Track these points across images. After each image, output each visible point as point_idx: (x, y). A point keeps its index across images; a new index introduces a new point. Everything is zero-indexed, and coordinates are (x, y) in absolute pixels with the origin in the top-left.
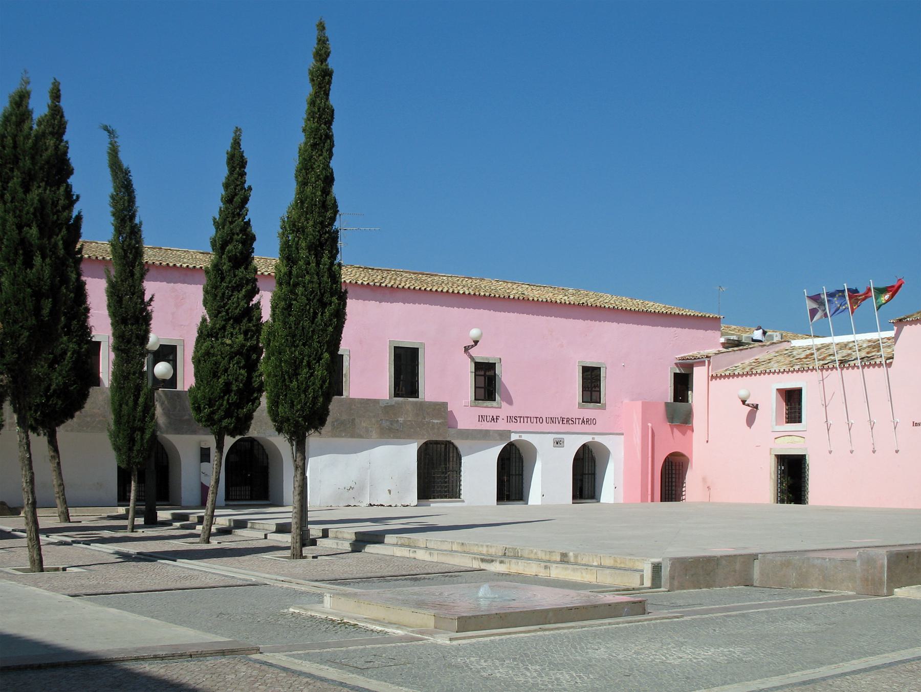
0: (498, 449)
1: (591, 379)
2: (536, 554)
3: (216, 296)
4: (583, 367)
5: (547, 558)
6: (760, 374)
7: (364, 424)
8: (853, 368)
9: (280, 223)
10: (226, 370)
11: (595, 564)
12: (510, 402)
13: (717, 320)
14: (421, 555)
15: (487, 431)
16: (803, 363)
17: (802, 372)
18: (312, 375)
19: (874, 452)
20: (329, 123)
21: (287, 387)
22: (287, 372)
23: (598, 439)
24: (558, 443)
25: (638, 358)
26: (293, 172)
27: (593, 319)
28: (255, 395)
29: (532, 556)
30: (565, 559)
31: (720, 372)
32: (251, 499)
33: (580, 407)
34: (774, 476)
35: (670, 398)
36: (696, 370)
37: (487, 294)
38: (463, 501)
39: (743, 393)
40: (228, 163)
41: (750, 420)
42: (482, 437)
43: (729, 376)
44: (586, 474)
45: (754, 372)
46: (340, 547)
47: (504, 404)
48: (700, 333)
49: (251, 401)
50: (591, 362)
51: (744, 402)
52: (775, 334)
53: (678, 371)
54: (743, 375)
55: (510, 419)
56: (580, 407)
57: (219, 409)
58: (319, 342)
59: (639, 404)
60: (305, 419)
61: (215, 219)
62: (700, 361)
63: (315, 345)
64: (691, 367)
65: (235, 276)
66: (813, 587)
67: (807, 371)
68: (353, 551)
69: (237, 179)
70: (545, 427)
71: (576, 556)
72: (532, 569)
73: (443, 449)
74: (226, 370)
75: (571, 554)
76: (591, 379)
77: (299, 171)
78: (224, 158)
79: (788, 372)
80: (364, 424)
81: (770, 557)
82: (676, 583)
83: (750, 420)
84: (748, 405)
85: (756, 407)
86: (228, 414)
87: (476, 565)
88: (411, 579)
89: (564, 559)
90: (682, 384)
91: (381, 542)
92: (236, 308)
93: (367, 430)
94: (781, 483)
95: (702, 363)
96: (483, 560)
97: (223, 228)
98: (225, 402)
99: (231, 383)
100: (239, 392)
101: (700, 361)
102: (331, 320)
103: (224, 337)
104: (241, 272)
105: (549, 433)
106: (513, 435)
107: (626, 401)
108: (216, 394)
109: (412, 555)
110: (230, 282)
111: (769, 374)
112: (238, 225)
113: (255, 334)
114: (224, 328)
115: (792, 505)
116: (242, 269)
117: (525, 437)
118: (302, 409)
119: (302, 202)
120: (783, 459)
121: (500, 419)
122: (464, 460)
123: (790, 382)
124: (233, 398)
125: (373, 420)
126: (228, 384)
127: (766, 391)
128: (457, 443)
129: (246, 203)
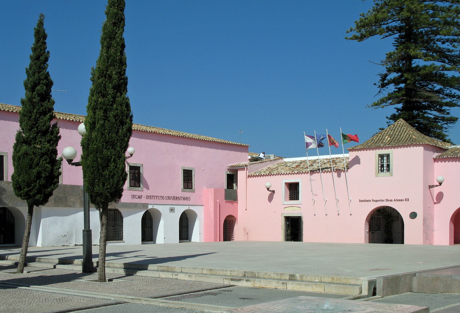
0: (142, 213)
1: (188, 176)
2: (269, 275)
3: (30, 117)
4: (184, 170)
5: (279, 277)
6: (275, 175)
7: (72, 200)
8: (327, 172)
9: (91, 71)
10: (38, 164)
11: (317, 281)
12: (148, 188)
13: (247, 147)
14: (181, 277)
15: (136, 204)
16: (298, 169)
17: (299, 174)
18: (116, 166)
19: (338, 215)
20: (122, 10)
21: (101, 175)
22: (101, 165)
23: (192, 208)
24: (172, 210)
25: (211, 165)
26: (99, 39)
27: (188, 144)
28: (56, 180)
29: (267, 276)
30: (293, 278)
31: (253, 173)
32: (4, 243)
33: (183, 191)
34: (284, 227)
35: (225, 187)
36: (239, 173)
37: (136, 129)
38: (124, 242)
39: (268, 185)
40: (35, 36)
41: (270, 198)
42: (134, 207)
43: (258, 176)
44: (185, 225)
45: (273, 174)
46: (116, 272)
47: (145, 189)
48: (239, 154)
49: (53, 184)
50: (188, 167)
51: (268, 189)
52: (271, 155)
53: (229, 173)
54: (265, 176)
55: (148, 197)
56: (183, 191)
57: (33, 188)
58: (120, 147)
59: (212, 190)
60: (111, 194)
61: (27, 69)
62: (242, 168)
63: (118, 149)
64: (236, 171)
65: (42, 106)
66: (454, 292)
67: (302, 174)
68: (127, 275)
69: (41, 46)
70: (165, 201)
71: (301, 276)
72: (272, 285)
73: (113, 214)
74: (38, 164)
75: (297, 275)
76: (188, 176)
77: (104, 39)
78: (33, 32)
79: (291, 174)
80: (72, 200)
81: (424, 275)
82: (385, 292)
83: (270, 198)
84: (270, 191)
85: (274, 192)
86: (39, 192)
87: (227, 282)
88: (212, 294)
89: (292, 278)
90: (232, 179)
91: (34, 261)
92: (44, 126)
93: (74, 202)
94: (287, 231)
95: (243, 169)
96: (232, 280)
97: (34, 75)
98: (37, 184)
99: (41, 172)
100: (46, 178)
101: (242, 168)
102: (126, 134)
103: (35, 143)
104: (45, 104)
105: (167, 205)
106: (149, 205)
107: (205, 188)
108: (32, 178)
109: (174, 277)
110: (38, 110)
111: (281, 175)
112: (43, 74)
113: (55, 142)
114: (35, 138)
115: (293, 242)
116: (46, 102)
117: (156, 207)
118: (111, 188)
119: (108, 59)
120: (287, 219)
121: (143, 197)
122: (124, 219)
123: (292, 179)
124: (43, 181)
125: (77, 197)
126: (39, 173)
127: (279, 184)
128: (122, 210)
129: (47, 61)
